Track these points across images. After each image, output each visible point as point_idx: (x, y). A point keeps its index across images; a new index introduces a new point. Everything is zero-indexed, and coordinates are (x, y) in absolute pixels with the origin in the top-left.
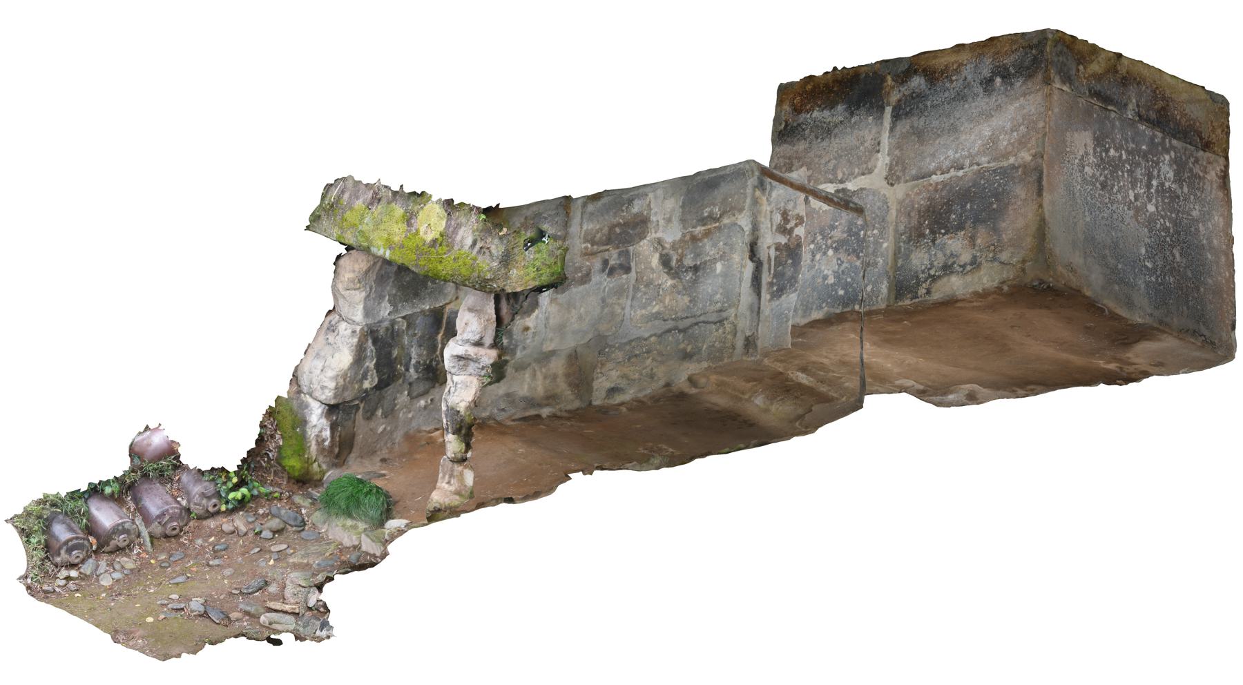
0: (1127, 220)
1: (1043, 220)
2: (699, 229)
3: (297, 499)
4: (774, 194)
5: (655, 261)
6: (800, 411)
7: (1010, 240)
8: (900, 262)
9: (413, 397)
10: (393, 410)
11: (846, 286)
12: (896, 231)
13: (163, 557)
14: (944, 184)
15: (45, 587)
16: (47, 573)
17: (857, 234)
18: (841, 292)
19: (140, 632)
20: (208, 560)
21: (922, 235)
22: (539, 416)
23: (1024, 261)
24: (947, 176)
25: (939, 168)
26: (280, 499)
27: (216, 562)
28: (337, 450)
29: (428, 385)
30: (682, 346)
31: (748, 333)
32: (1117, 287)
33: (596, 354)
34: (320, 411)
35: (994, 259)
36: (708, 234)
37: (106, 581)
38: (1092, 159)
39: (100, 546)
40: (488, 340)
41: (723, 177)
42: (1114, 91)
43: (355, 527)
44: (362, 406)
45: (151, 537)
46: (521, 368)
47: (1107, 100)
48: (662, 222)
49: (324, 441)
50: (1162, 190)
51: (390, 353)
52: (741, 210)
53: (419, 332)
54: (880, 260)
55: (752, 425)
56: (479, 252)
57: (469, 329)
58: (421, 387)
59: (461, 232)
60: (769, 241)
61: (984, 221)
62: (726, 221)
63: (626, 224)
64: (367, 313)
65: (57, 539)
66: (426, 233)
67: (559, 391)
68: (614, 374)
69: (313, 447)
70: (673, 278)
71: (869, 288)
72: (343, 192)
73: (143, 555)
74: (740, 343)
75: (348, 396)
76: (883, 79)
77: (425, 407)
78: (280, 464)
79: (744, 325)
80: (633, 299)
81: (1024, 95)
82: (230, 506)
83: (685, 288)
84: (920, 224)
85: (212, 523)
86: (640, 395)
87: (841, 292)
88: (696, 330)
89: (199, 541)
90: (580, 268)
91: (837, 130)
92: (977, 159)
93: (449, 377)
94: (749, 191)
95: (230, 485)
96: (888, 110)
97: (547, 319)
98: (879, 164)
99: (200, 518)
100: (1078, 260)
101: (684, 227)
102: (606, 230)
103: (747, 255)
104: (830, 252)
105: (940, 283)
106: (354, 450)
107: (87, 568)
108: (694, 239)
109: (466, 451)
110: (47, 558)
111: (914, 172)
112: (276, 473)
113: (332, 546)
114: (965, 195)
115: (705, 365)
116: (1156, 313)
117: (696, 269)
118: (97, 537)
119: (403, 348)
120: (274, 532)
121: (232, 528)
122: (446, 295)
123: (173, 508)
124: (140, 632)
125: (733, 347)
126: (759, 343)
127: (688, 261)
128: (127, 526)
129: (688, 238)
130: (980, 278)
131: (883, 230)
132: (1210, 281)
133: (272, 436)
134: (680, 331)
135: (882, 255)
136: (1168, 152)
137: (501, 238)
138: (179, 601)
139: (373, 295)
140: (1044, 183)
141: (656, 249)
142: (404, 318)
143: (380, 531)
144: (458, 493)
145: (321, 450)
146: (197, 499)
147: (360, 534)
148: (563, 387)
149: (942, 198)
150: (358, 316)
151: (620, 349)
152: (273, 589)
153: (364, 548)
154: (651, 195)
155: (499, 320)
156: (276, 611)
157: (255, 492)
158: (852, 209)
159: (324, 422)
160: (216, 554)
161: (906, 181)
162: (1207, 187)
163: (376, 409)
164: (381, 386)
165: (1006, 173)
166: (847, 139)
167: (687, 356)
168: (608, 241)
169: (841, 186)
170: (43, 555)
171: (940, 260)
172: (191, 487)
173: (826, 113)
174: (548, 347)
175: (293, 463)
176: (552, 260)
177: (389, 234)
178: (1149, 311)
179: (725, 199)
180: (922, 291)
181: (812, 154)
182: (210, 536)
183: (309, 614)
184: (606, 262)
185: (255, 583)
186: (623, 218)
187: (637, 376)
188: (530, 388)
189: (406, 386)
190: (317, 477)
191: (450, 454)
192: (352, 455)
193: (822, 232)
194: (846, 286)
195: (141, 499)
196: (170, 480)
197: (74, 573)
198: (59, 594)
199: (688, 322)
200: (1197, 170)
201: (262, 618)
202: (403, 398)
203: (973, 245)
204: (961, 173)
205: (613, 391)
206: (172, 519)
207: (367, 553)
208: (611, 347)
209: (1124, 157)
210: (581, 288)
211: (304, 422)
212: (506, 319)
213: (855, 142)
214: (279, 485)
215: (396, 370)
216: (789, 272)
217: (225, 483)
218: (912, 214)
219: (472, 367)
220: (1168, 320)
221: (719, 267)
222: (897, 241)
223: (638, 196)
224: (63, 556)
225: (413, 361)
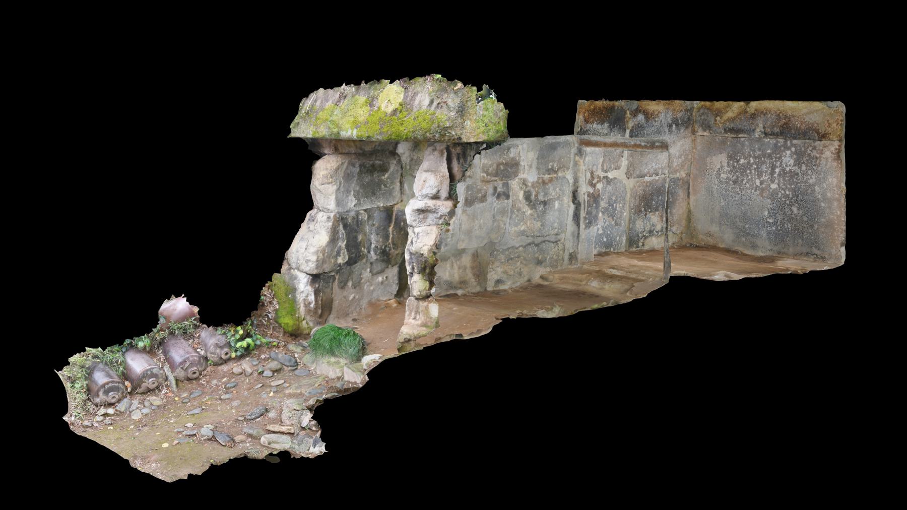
0: (754, 197)
1: (690, 211)
2: (547, 177)
3: (291, 347)
4: (587, 159)
5: (521, 195)
6: (626, 287)
9: (374, 274)
10: (359, 282)
13: (185, 395)
14: (650, 183)
15: (86, 423)
16: (88, 411)
18: (605, 240)
19: (156, 457)
20: (221, 395)
21: (640, 211)
22: (456, 295)
24: (651, 178)
25: (648, 173)
26: (278, 347)
27: (227, 396)
28: (320, 311)
29: (383, 265)
30: (537, 255)
31: (571, 251)
32: (744, 239)
34: (306, 280)
36: (551, 180)
37: (136, 416)
38: (726, 169)
39: (134, 389)
40: (444, 193)
42: (746, 125)
43: (338, 363)
44: (337, 277)
45: (177, 380)
46: (445, 259)
47: (737, 131)
48: (527, 167)
49: (310, 303)
50: (783, 173)
51: (356, 237)
52: (568, 168)
55: (597, 296)
56: (437, 107)
57: (427, 185)
58: (378, 267)
59: (418, 98)
63: (506, 164)
64: (339, 203)
65: (96, 384)
66: (387, 107)
68: (499, 270)
69: (302, 309)
70: (532, 209)
72: (316, 101)
73: (170, 394)
74: (566, 257)
75: (327, 268)
76: (625, 113)
77: (382, 283)
78: (277, 322)
79: (570, 246)
81: (684, 138)
82: (239, 354)
83: (538, 216)
85: (225, 368)
86: (514, 286)
89: (215, 382)
93: (410, 230)
94: (572, 156)
95: (238, 337)
96: (628, 131)
97: (461, 224)
98: (623, 164)
99: (215, 364)
100: (714, 229)
101: (539, 174)
102: (495, 166)
103: (571, 199)
106: (333, 312)
107: (122, 407)
108: (544, 182)
109: (430, 288)
110: (89, 399)
112: (274, 329)
113: (320, 379)
115: (548, 269)
116: (776, 248)
117: (545, 203)
118: (132, 382)
119: (365, 234)
120: (274, 372)
121: (240, 371)
122: (394, 197)
123: (193, 357)
124: (156, 457)
125: (563, 260)
126: (579, 256)
127: (541, 198)
128: (155, 371)
131: (624, 204)
132: (823, 220)
133: (271, 303)
136: (789, 149)
137: (456, 92)
138: (193, 429)
139: (342, 189)
140: (691, 190)
141: (521, 188)
142: (365, 210)
143: (358, 364)
144: (424, 325)
145: (308, 311)
146: (212, 349)
147: (342, 367)
148: (469, 276)
150: (332, 205)
151: (503, 253)
152: (272, 414)
153: (346, 378)
155: (452, 178)
156: (274, 432)
157: (258, 343)
158: (657, 147)
159: (309, 290)
160: (227, 390)
162: (823, 162)
163: (347, 281)
164: (351, 262)
165: (674, 181)
167: (539, 263)
168: (496, 175)
169: (606, 175)
170: (85, 396)
172: (207, 341)
174: (461, 246)
175: (287, 321)
176: (496, 120)
177: (355, 118)
178: (769, 248)
179: (560, 159)
180: (640, 244)
182: (223, 378)
183: (303, 433)
184: (495, 189)
185: (257, 410)
186: (505, 159)
187: (512, 273)
190: (306, 332)
191: (415, 292)
192: (331, 316)
195: (169, 352)
196: (193, 336)
197: (111, 411)
198: (97, 427)
199: (540, 240)
200: (815, 153)
201: (263, 439)
202: (367, 274)
204: (657, 178)
205: (498, 282)
206: (192, 365)
207: (349, 382)
208: (498, 251)
209: (752, 161)
210: (481, 205)
211: (294, 290)
212: (458, 175)
214: (277, 337)
215: (361, 251)
217: (233, 335)
219: (431, 217)
220: (785, 250)
221: (557, 204)
222: (630, 213)
224: (102, 397)
225: (373, 246)
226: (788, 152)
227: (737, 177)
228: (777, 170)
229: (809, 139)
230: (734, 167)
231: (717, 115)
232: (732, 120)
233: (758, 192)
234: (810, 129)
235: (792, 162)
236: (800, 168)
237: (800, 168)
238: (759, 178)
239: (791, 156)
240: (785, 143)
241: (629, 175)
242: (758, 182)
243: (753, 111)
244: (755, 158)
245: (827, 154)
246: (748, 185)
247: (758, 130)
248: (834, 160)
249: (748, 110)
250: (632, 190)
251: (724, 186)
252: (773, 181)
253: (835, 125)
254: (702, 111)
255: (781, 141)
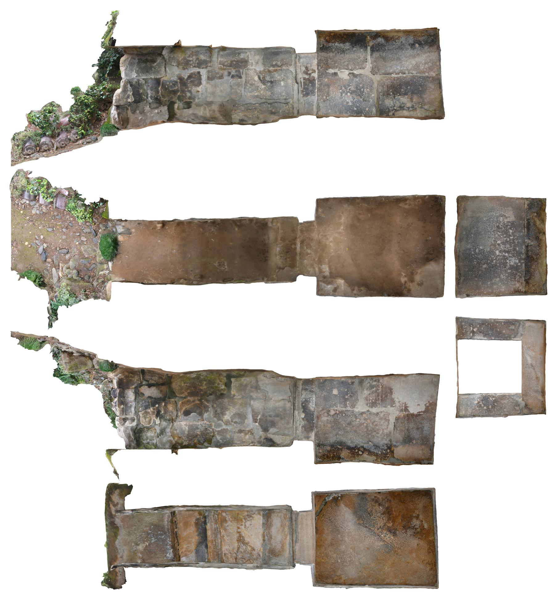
5: (256, 78)
7: (428, 102)
8: (380, 103)
11: (357, 107)
12: (377, 91)
14: (398, 78)
17: (360, 89)
18: (355, 109)
21: (389, 94)
23: (435, 110)
24: (399, 76)
30: (270, 109)
33: (232, 106)
35: (421, 107)
36: (276, 71)
41: (281, 52)
48: (254, 63)
51: (138, 91)
52: (291, 65)
53: (150, 85)
58: (155, 105)
60: (301, 76)
61: (416, 94)
62: (284, 68)
63: (238, 61)
67: (216, 116)
69: (113, 121)
71: (367, 109)
76: (366, 37)
77: (158, 113)
80: (245, 88)
84: (388, 91)
87: (355, 109)
88: (276, 105)
90: (218, 73)
91: (347, 52)
92: (411, 71)
96: (369, 48)
98: (367, 66)
102: (229, 62)
104: (349, 94)
106: (130, 124)
108: (269, 71)
111: (383, 72)
114: (407, 84)
129: (266, 70)
130: (417, 114)
131: (371, 90)
134: (269, 104)
135: (372, 98)
139: (128, 69)
142: (143, 79)
154: (248, 53)
165: (425, 78)
166: (353, 56)
171: (398, 104)
173: (342, 45)
174: (209, 100)
181: (337, 58)
188: (203, 113)
189: (148, 104)
193: (344, 86)
194: (357, 107)
202: (147, 108)
203: (412, 101)
204: (405, 75)
210: (220, 80)
213: (356, 57)
216: (310, 88)
221: (282, 83)
222: (378, 95)
223: (243, 52)
225: (149, 95)
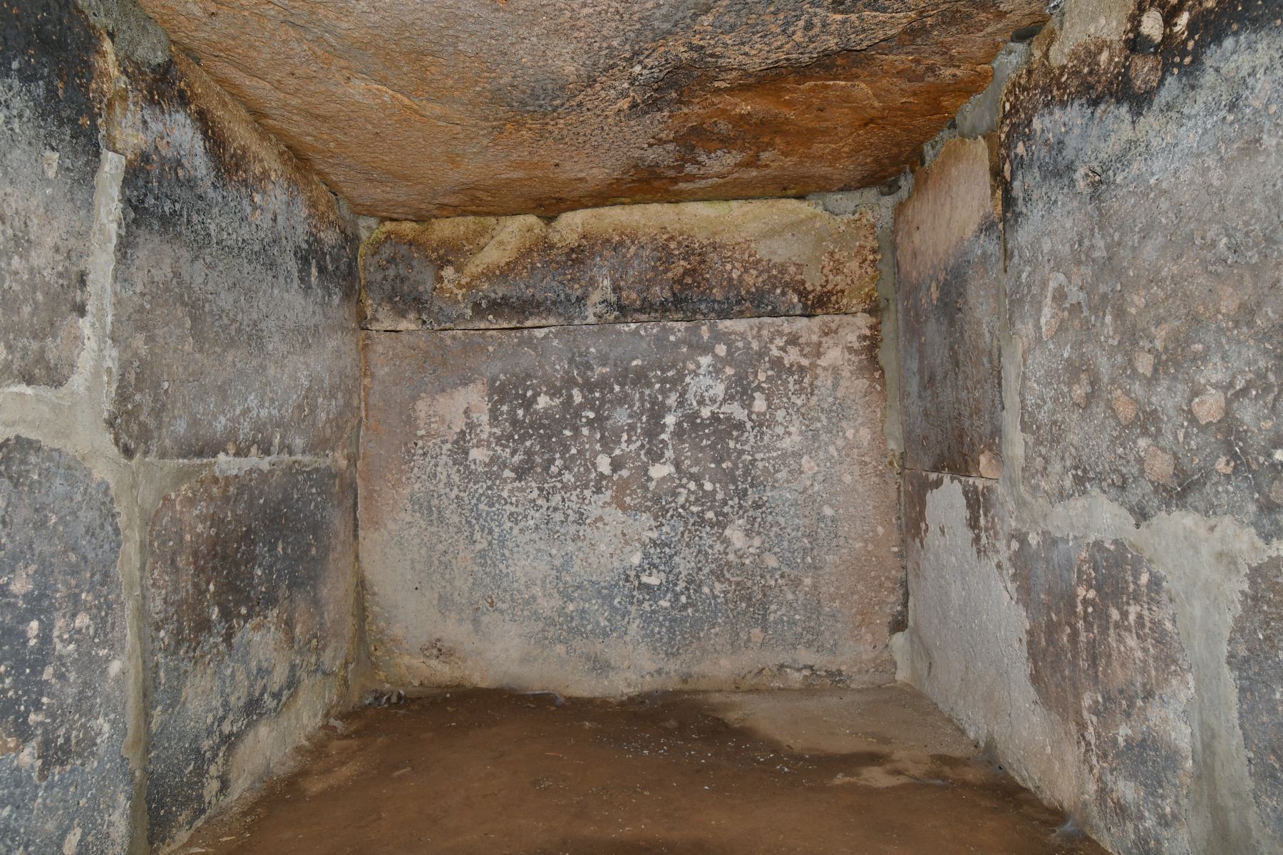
21: (203, 625)
24: (246, 463)
25: (232, 435)
42: (547, 287)
50: (691, 425)
54: (103, 725)
98: (85, 360)
105: (243, 749)
131: (104, 613)
136: (707, 349)
149: (238, 519)
161: (163, 455)
209: (578, 398)
218: (181, 561)
222: (146, 654)
226: (705, 361)
227: (529, 453)
228: (670, 420)
229: (774, 314)
230: (514, 422)
231: (443, 262)
232: (503, 273)
233: (608, 495)
234: (773, 282)
235: (719, 389)
236: (747, 404)
237: (747, 404)
238: (607, 449)
239: (716, 371)
240: (695, 331)
241: (130, 428)
242: (604, 464)
243: (572, 239)
244: (588, 387)
245: (833, 355)
246: (568, 477)
247: (596, 297)
248: (860, 371)
249: (555, 238)
250: (150, 521)
251: (481, 487)
252: (656, 457)
253: (854, 264)
254: (387, 251)
255: (679, 328)
